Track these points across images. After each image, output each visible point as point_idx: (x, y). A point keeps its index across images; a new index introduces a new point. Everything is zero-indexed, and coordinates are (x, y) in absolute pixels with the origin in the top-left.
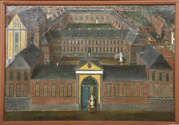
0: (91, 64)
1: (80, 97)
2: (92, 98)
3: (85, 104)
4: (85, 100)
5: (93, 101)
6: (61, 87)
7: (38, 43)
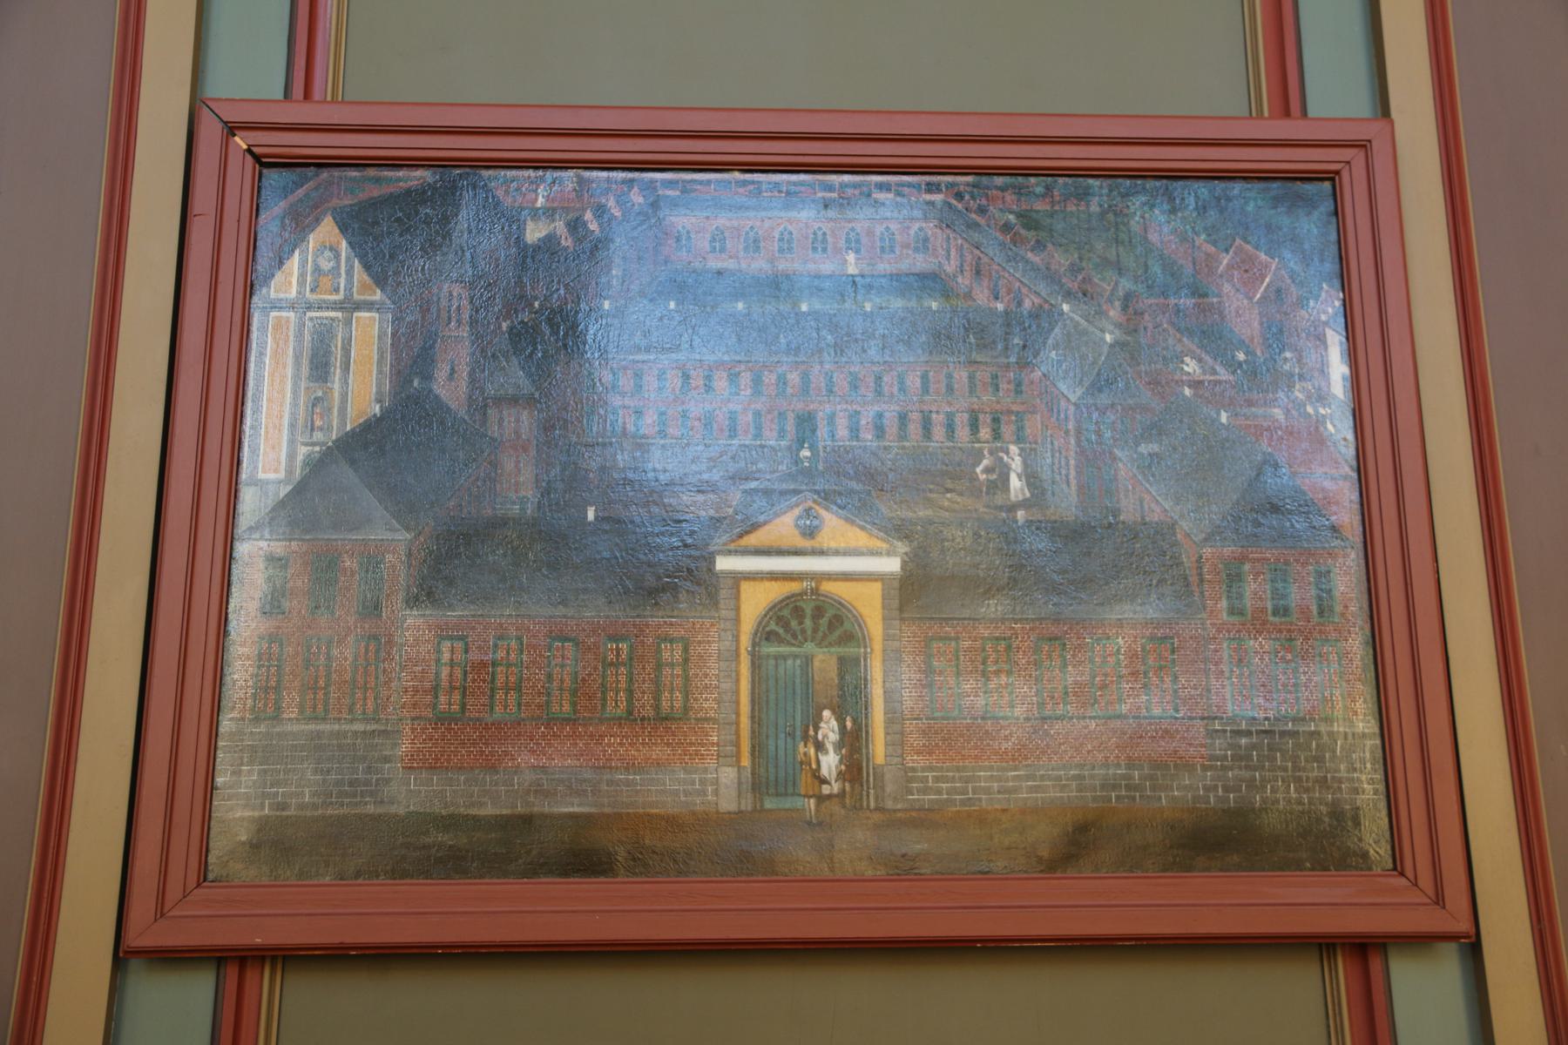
0: (823, 512)
1: (745, 722)
2: (829, 729)
3: (781, 763)
4: (781, 743)
5: (839, 746)
6: (611, 657)
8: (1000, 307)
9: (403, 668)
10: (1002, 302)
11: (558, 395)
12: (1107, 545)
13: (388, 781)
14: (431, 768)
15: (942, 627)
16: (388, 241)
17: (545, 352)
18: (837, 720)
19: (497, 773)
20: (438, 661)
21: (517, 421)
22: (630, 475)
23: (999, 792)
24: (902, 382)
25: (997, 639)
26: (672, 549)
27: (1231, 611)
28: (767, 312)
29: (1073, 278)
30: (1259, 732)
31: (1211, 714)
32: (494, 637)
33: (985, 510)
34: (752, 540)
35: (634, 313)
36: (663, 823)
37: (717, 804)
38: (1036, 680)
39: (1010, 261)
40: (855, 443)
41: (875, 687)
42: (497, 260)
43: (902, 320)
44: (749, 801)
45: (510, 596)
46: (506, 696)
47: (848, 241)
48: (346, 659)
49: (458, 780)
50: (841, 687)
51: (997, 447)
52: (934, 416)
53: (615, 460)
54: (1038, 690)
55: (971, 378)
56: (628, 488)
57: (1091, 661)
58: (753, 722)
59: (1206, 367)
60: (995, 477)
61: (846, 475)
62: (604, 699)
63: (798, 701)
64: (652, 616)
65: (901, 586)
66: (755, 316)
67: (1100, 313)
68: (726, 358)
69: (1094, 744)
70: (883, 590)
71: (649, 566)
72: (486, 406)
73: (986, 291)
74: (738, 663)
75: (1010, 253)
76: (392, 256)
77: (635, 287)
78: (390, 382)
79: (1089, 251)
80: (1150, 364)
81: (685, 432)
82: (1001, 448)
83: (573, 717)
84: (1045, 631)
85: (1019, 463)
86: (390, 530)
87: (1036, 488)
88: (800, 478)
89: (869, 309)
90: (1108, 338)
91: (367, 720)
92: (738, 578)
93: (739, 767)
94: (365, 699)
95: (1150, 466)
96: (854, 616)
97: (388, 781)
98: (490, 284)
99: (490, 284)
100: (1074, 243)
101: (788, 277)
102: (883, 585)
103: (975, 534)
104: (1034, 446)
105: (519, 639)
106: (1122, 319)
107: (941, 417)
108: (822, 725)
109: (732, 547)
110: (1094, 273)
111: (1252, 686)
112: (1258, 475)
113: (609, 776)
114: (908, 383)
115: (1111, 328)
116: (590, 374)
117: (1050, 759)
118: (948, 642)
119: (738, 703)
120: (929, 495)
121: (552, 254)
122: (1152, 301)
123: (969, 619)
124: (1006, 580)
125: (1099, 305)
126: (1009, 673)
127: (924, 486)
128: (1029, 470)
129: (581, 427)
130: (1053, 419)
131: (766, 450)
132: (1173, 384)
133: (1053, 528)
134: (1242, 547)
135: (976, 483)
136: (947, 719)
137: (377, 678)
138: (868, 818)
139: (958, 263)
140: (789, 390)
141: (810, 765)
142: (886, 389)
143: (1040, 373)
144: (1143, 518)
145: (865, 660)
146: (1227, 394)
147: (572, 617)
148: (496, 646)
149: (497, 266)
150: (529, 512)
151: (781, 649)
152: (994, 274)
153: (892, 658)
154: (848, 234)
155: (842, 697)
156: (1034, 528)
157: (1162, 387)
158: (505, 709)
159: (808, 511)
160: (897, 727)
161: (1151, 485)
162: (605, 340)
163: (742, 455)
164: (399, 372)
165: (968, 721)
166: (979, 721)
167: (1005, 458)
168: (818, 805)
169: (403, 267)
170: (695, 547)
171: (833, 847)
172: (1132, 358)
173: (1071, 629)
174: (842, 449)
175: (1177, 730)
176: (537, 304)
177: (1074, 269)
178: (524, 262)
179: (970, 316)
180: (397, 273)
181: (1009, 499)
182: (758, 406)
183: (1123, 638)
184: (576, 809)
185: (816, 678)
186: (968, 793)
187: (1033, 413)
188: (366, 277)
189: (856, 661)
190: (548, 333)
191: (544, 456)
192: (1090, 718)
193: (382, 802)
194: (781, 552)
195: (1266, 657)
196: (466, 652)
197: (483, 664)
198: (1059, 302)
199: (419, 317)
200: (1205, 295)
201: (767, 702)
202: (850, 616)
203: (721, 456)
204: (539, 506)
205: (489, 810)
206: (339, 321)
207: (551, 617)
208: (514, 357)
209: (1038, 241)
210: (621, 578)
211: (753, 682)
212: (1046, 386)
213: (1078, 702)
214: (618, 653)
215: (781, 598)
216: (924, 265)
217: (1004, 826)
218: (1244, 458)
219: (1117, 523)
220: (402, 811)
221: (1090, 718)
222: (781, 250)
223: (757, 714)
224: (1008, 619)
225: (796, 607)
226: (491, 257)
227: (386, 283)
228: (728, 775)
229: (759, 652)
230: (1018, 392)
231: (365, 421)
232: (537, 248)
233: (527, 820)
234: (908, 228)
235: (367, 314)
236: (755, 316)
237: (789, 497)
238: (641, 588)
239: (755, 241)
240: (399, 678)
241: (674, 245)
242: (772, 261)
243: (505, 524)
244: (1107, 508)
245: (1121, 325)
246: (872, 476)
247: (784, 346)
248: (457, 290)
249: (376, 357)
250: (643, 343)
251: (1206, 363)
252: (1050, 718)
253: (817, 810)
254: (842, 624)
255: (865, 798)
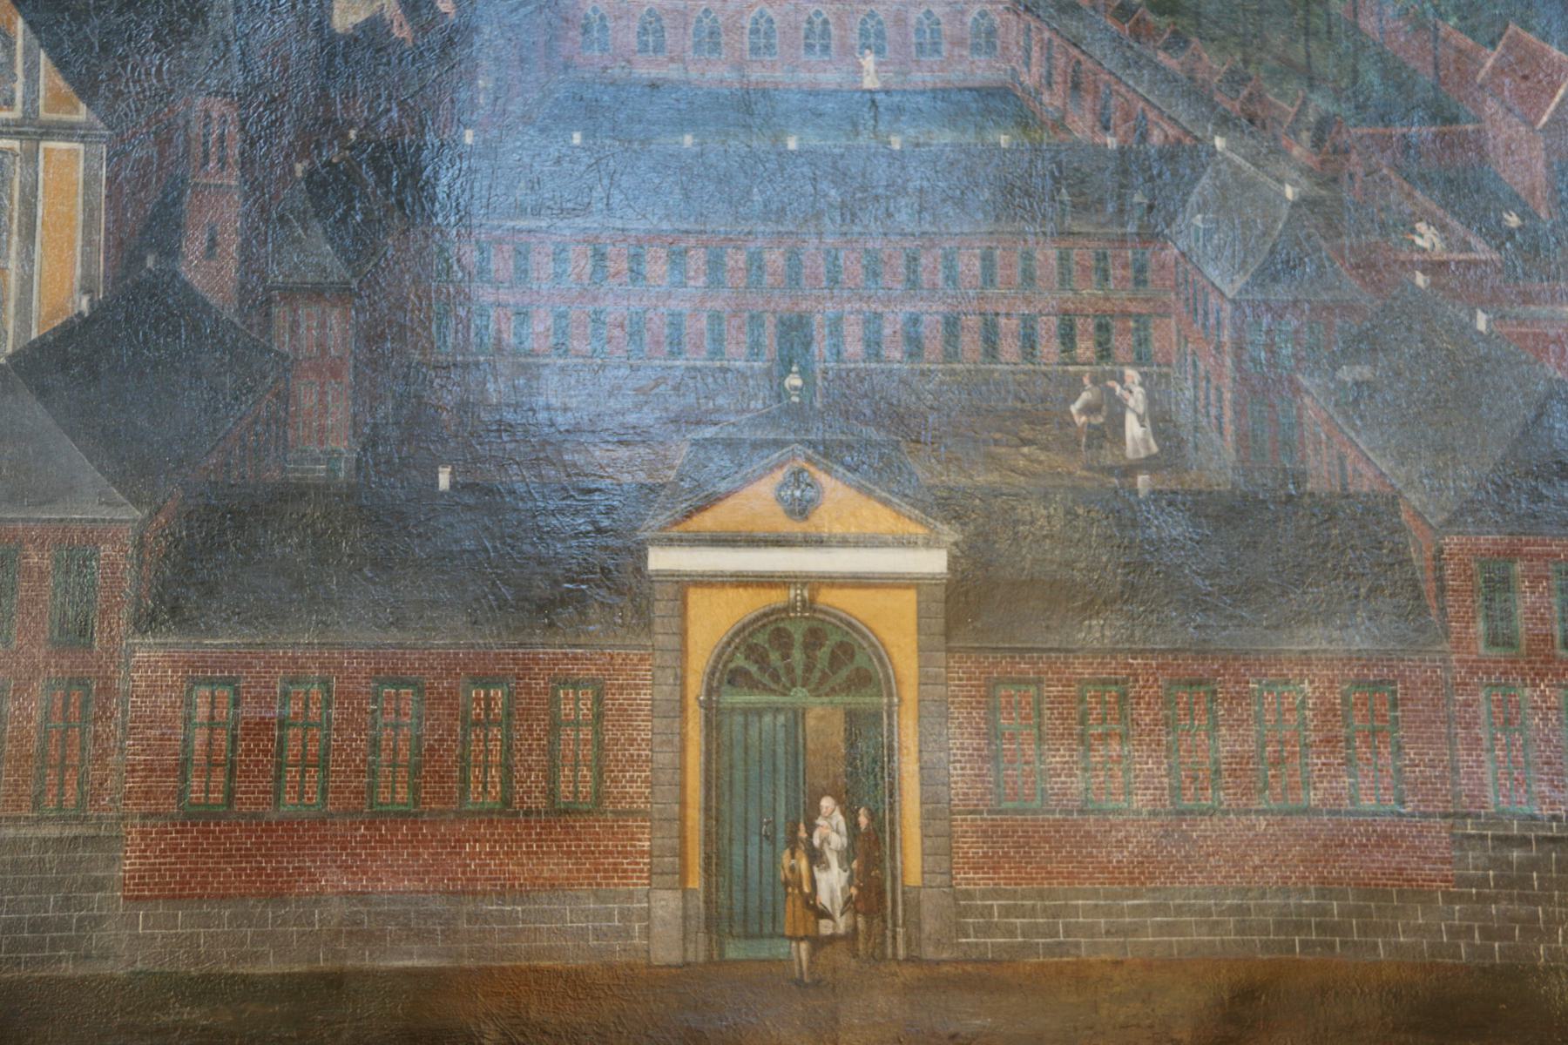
0: (823, 478)
1: (695, 817)
2: (831, 828)
3: (753, 884)
4: (753, 852)
5: (846, 857)
6: (477, 711)
7: (232, 266)
8: (1112, 142)
9: (128, 732)
10: (1115, 135)
11: (389, 285)
12: (1285, 530)
13: (98, 921)
14: (174, 897)
15: (1013, 664)
16: (97, 22)
17: (367, 213)
18: (843, 813)
19: (286, 903)
20: (188, 720)
21: (322, 325)
22: (509, 416)
23: (1108, 933)
24: (950, 267)
25: (1104, 682)
26: (576, 536)
27: (1493, 641)
28: (731, 150)
29: (1233, 94)
30: (1541, 840)
31: (1460, 810)
32: (283, 679)
33: (1085, 473)
34: (706, 521)
35: (513, 151)
36: (560, 983)
37: (648, 952)
38: (1168, 749)
39: (1129, 66)
40: (873, 365)
41: (905, 759)
42: (286, 58)
43: (952, 164)
44: (701, 948)
45: (309, 613)
46: (303, 776)
47: (864, 34)
48: (29, 718)
49: (220, 917)
50: (851, 760)
51: (1104, 371)
52: (1002, 321)
53: (483, 391)
54: (1171, 767)
55: (1063, 258)
56: (505, 437)
57: (1259, 719)
58: (708, 817)
59: (1453, 240)
60: (1101, 419)
61: (859, 416)
62: (465, 780)
63: (781, 782)
64: (543, 645)
65: (948, 597)
66: (712, 159)
67: (1277, 151)
68: (665, 226)
69: (1265, 856)
70: (919, 603)
71: (540, 564)
72: (269, 301)
73: (1089, 116)
74: (684, 722)
75: (1129, 54)
76: (105, 48)
77: (515, 108)
78: (106, 259)
79: (1260, 49)
80: (1358, 236)
81: (596, 344)
82: (1112, 372)
83: (413, 810)
84: (1181, 671)
85: (1140, 397)
86: (108, 504)
87: (1168, 438)
88: (785, 421)
89: (897, 147)
90: (1289, 192)
91: (64, 820)
92: (685, 583)
93: (685, 891)
94: (62, 784)
95: (1356, 401)
96: (872, 645)
97: (98, 921)
98: (274, 100)
99: (274, 100)
100: (1235, 34)
101: (765, 93)
102: (919, 594)
103: (1068, 512)
104: (1165, 369)
105: (325, 682)
106: (1313, 161)
107: (1014, 323)
108: (820, 821)
109: (674, 532)
110: (1267, 86)
111: (1528, 763)
112: (1539, 416)
113: (471, 907)
114: (961, 267)
115: (1295, 175)
116: (442, 250)
117: (1192, 879)
118: (1023, 688)
119: (683, 786)
120: (993, 448)
121: (378, 51)
122: (1364, 130)
123: (1058, 650)
124: (1118, 587)
125: (1275, 138)
126: (1123, 738)
127: (985, 435)
128: (1157, 408)
129: (428, 338)
130: (1197, 326)
131: (729, 375)
132: (1396, 267)
133: (1195, 503)
134: (1511, 534)
135: (1071, 431)
136: (1024, 812)
137: (83, 749)
138: (895, 974)
139: (1043, 71)
140: (768, 280)
141: (800, 887)
142: (924, 277)
143: (1176, 251)
144: (1344, 488)
145: (890, 716)
146: (1488, 283)
147: (413, 647)
148: (285, 694)
149: (286, 70)
150: (342, 475)
151: (753, 698)
152: (1102, 88)
153: (933, 713)
154: (864, 22)
155: (852, 775)
156: (1164, 503)
157: (1379, 272)
158: (301, 797)
159: (797, 474)
160: (940, 825)
161: (1358, 432)
162: (467, 195)
163: (691, 383)
164: (121, 242)
165: (1057, 816)
166: (1075, 816)
167: (1118, 389)
168: (813, 953)
169: (124, 67)
170: (616, 534)
171: (837, 1022)
172: (1330, 225)
173: (1224, 666)
174: (853, 375)
175: (1402, 835)
176: (353, 134)
177: (1235, 79)
178: (330, 62)
179: (1063, 157)
180: (113, 77)
181: (1125, 457)
182: (718, 305)
183: (1311, 682)
184: (416, 963)
185: (810, 745)
186: (1057, 934)
187: (1165, 315)
188: (60, 82)
189: (877, 716)
190: (371, 181)
191: (367, 383)
192: (1258, 812)
193: (88, 957)
194: (753, 542)
195: (1552, 715)
196: (236, 704)
197: (264, 725)
198: (1209, 134)
199: (154, 151)
200: (1455, 119)
201: (731, 783)
202: (865, 645)
203: (657, 385)
204: (359, 466)
205: (271, 966)
206: (15, 155)
207: (378, 647)
208: (315, 222)
209: (1175, 33)
210: (494, 583)
211: (708, 753)
212: (1186, 272)
213: (1238, 787)
214: (488, 705)
215: (752, 616)
216: (988, 74)
217: (1117, 989)
218: (1515, 388)
219: (1301, 496)
220: (121, 971)
221: (1258, 812)
222: (755, 50)
223: (714, 804)
224: (1121, 651)
225: (778, 629)
226: (274, 55)
227: (96, 93)
228: (666, 904)
229: (718, 702)
230: (1140, 282)
231: (64, 324)
232: (352, 41)
233: (335, 982)
234: (963, 12)
235: (63, 145)
236: (712, 159)
237: (766, 452)
238: (526, 599)
239: (712, 34)
240: (122, 750)
241: (580, 39)
242: (739, 66)
243: (303, 495)
244: (1285, 470)
245: (1311, 170)
246: (902, 419)
247: (758, 207)
248: (217, 107)
249: (81, 217)
250: (530, 200)
251: (1453, 232)
252: (1191, 812)
253: (811, 962)
254: (852, 656)
255: (889, 941)
